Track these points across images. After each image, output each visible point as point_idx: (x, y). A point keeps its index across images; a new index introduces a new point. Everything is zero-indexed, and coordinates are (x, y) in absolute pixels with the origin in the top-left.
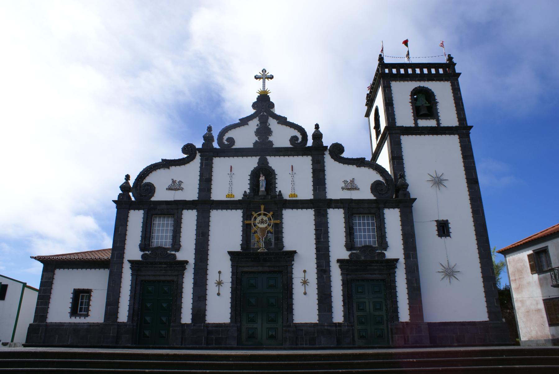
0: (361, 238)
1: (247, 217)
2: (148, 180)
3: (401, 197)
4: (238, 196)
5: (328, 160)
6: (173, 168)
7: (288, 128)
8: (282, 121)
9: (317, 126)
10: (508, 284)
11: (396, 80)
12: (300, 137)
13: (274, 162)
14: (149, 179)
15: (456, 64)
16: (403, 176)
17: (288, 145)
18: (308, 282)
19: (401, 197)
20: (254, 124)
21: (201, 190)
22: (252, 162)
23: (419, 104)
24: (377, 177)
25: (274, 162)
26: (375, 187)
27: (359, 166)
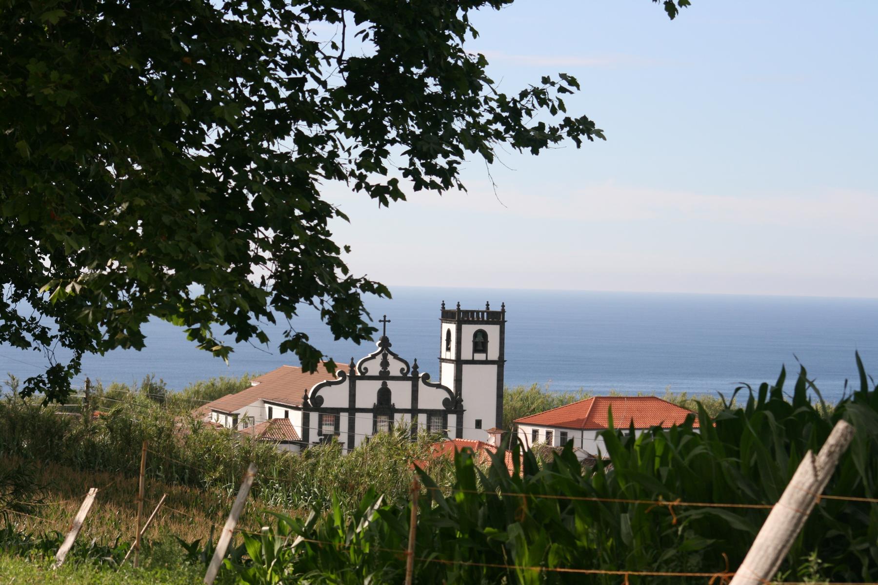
0: (331, 420)
1: (375, 417)
2: (318, 394)
3: (458, 409)
4: (371, 406)
5: (420, 382)
6: (333, 386)
7: (394, 352)
8: (396, 356)
9: (415, 360)
10: (311, 129)
11: (465, 324)
12: (406, 369)
13: (391, 384)
14: (319, 394)
15: (498, 8)
16: (460, 395)
17: (399, 374)
18: (598, 439)
19: (458, 409)
20: (379, 358)
21: (350, 401)
22: (378, 384)
23: (477, 340)
24: (446, 395)
25: (391, 384)
26: (445, 402)
27: (437, 388)
